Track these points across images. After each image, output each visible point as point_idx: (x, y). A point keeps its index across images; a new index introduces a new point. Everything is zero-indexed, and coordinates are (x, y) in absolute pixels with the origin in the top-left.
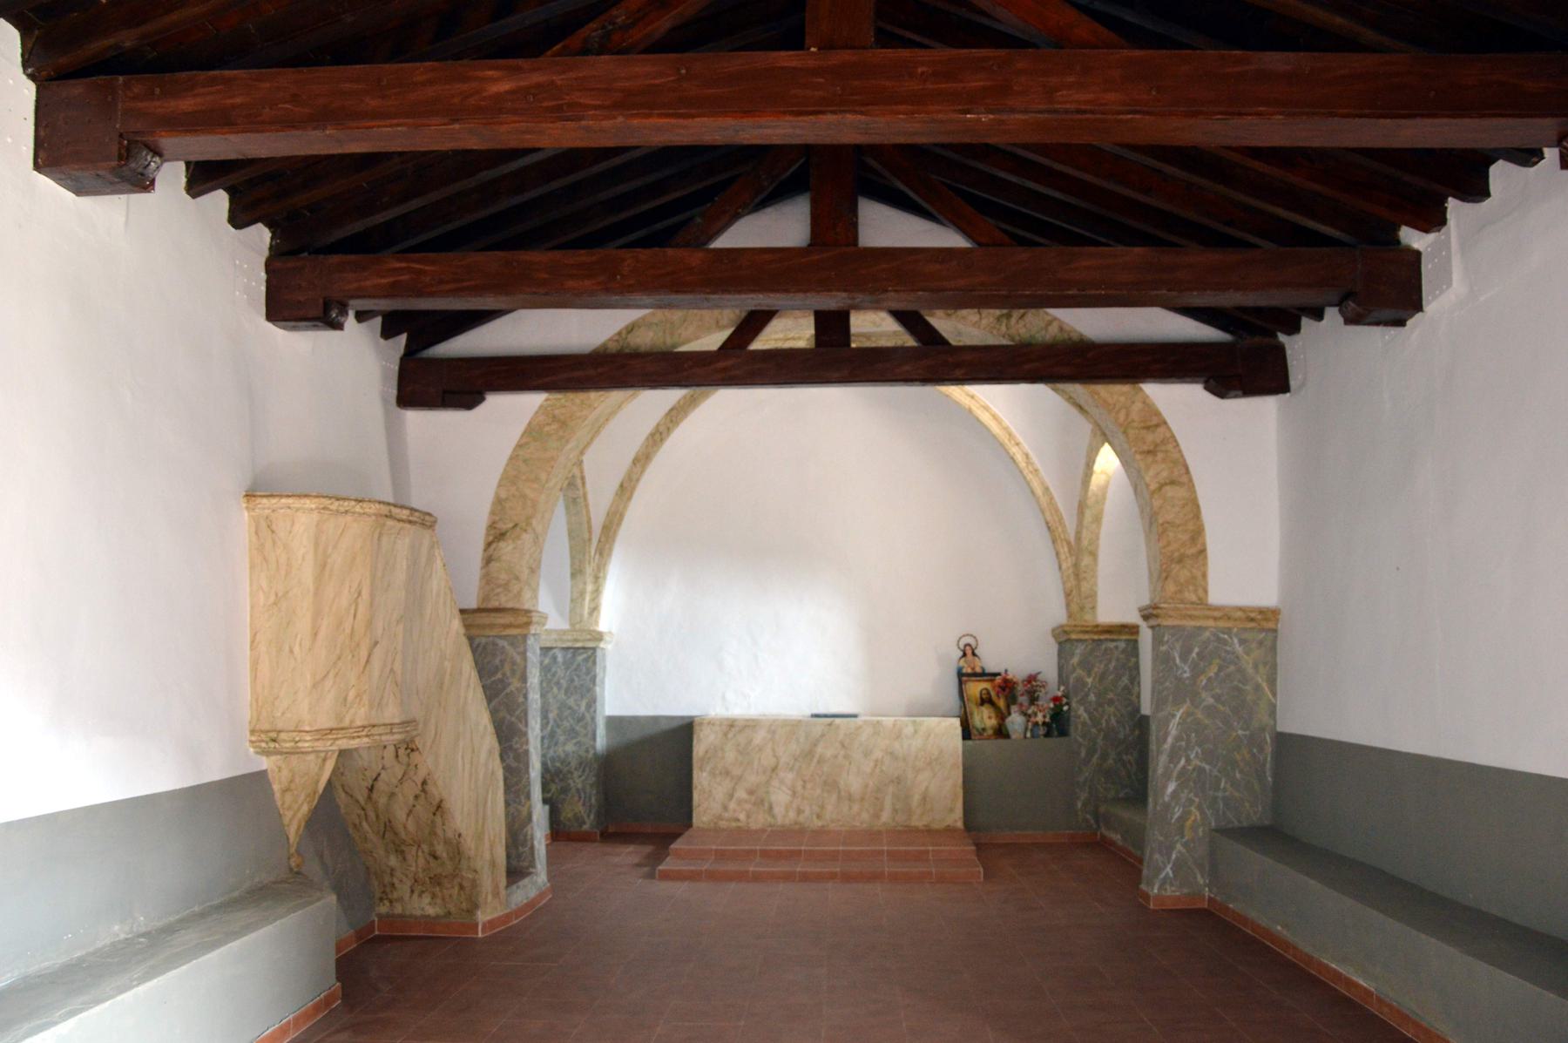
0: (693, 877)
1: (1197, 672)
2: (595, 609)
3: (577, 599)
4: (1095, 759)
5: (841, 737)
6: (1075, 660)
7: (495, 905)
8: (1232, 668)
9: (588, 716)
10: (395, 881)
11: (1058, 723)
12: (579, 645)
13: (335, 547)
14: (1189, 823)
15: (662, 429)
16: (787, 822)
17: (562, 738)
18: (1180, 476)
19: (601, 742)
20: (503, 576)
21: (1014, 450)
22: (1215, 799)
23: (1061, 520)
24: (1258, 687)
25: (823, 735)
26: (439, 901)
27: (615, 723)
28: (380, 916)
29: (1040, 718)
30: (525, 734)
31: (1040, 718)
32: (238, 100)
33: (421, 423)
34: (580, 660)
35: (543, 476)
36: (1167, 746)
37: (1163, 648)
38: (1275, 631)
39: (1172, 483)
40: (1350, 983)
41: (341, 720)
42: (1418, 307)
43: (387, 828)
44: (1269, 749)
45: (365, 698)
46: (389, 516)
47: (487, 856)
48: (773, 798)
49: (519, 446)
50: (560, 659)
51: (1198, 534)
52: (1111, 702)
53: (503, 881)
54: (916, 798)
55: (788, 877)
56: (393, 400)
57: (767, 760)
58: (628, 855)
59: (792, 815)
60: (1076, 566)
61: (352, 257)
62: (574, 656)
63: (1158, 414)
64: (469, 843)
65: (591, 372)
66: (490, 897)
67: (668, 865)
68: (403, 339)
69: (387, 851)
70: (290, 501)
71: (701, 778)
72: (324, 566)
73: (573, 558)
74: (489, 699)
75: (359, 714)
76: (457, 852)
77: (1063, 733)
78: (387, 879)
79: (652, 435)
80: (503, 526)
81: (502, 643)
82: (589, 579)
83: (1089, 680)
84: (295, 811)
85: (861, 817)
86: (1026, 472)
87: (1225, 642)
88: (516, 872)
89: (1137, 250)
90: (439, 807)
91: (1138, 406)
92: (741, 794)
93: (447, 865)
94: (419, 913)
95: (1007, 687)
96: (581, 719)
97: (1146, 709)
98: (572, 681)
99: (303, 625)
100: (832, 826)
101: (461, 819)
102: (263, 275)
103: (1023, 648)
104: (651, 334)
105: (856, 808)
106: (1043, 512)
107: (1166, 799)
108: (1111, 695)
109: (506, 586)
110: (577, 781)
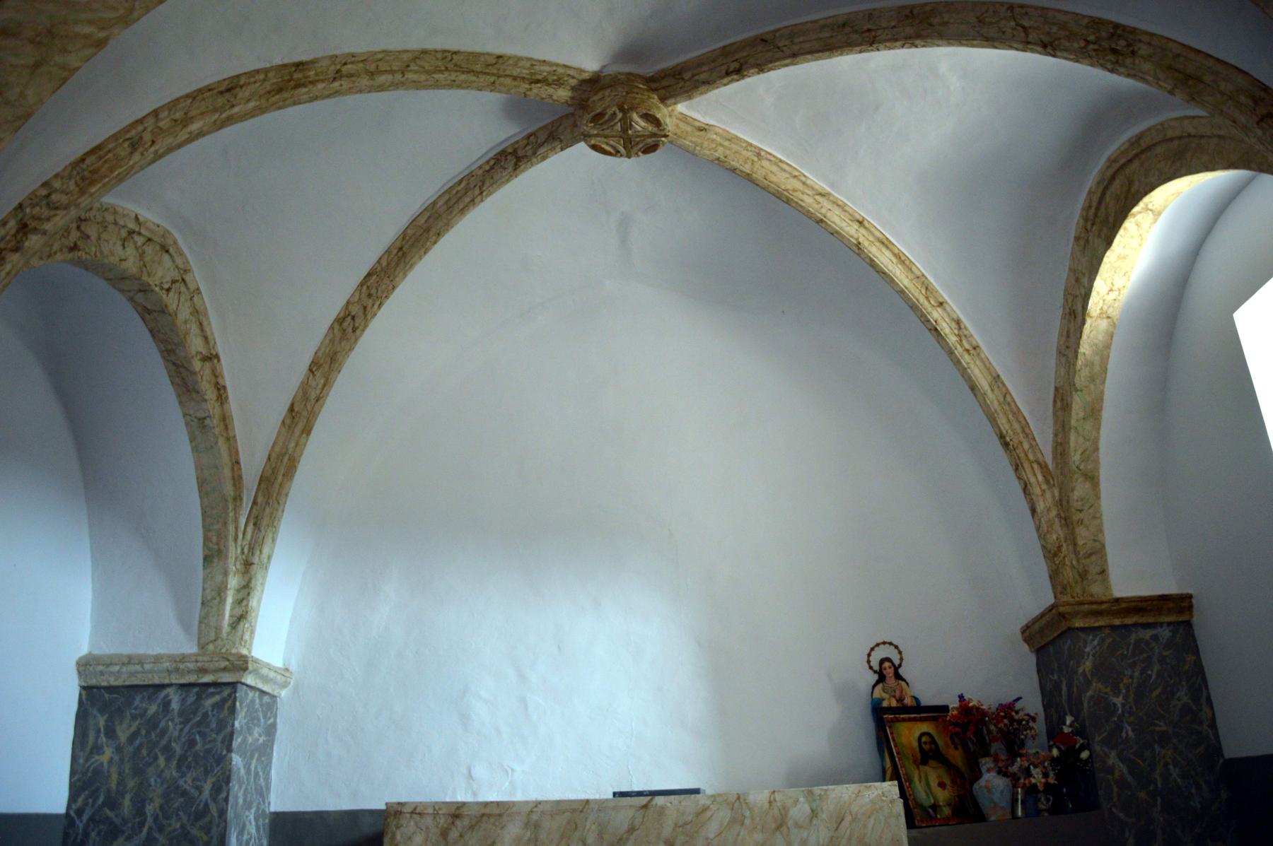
2: (241, 618)
5: (667, 831)
6: (1087, 665)
9: (214, 810)
11: (1073, 784)
12: (207, 679)
15: (355, 310)
21: (936, 315)
23: (1025, 427)
25: (632, 830)
31: (1037, 777)
50: (175, 705)
60: (1063, 504)
62: (199, 697)
73: (206, 529)
79: (340, 321)
82: (233, 565)
83: (1118, 701)
86: (959, 351)
98: (192, 743)
103: (971, 656)
106: (992, 419)
108: (1162, 727)
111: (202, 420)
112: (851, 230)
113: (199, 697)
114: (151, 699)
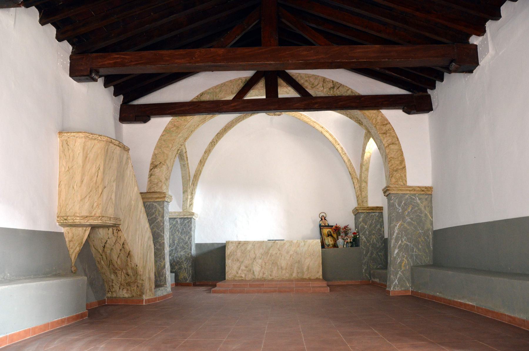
0: (224, 292)
1: (404, 210)
2: (191, 205)
3: (185, 201)
4: (369, 255)
6: (361, 220)
8: (417, 208)
9: (189, 242)
10: (114, 284)
11: (355, 242)
13: (91, 151)
14: (403, 264)
15: (214, 141)
16: (259, 277)
17: (179, 250)
18: (395, 141)
19: (194, 252)
20: (156, 181)
21: (337, 146)
22: (412, 256)
23: (354, 170)
24: (426, 215)
25: (272, 246)
26: (129, 292)
27: (199, 246)
28: (108, 298)
29: (349, 240)
30: (163, 237)
31: (349, 240)
33: (128, 128)
34: (186, 222)
35: (171, 146)
36: (394, 236)
37: (392, 202)
38: (431, 195)
39: (393, 144)
40: (465, 305)
41: (91, 213)
42: (477, 64)
43: (110, 263)
44: (431, 237)
45: (101, 207)
46: (111, 142)
47: (147, 276)
48: (254, 269)
49: (162, 135)
50: (179, 222)
51: (402, 161)
53: (153, 286)
54: (306, 268)
55: (259, 292)
57: (253, 256)
59: (261, 275)
60: (360, 187)
61: (101, 54)
62: (184, 220)
63: (387, 120)
64: (140, 269)
65: (187, 108)
66: (148, 291)
68: (121, 97)
69: (111, 273)
70: (75, 134)
71: (228, 262)
72: (86, 157)
74: (150, 225)
75: (98, 212)
77: (357, 246)
78: (111, 284)
79: (211, 143)
80: (156, 163)
81: (155, 204)
83: (366, 227)
85: (286, 275)
87: (414, 199)
89: (378, 46)
90: (129, 254)
91: (380, 117)
92: (243, 267)
93: (132, 278)
94: (122, 296)
95: (337, 229)
96: (187, 242)
97: (386, 236)
98: (183, 229)
99: (78, 178)
101: (137, 259)
102: (69, 61)
103: (342, 216)
104: (209, 96)
105: (284, 272)
106: (348, 168)
107: (395, 256)
108: (374, 232)
110: (185, 265)
111: (184, 165)
112: (320, 129)
113: (184, 220)
114: (174, 221)
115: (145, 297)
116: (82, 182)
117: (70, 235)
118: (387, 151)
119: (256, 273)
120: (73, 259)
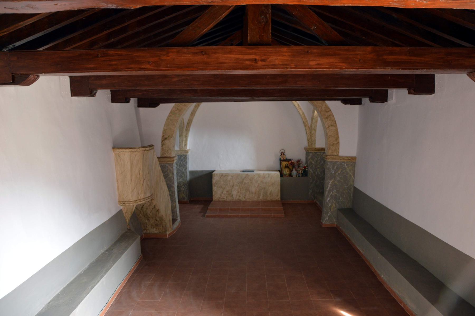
0: (214, 217)
2: (186, 145)
6: (310, 157)
7: (171, 229)
11: (305, 173)
18: (334, 124)
23: (307, 121)
24: (350, 175)
27: (192, 172)
28: (144, 233)
29: (300, 172)
32: (116, 81)
34: (183, 158)
39: (332, 126)
40: (360, 252)
44: (352, 190)
48: (233, 193)
49: (169, 116)
51: (337, 138)
52: (318, 168)
53: (172, 224)
56: (137, 106)
58: (197, 208)
59: (238, 197)
60: (310, 133)
63: (329, 108)
67: (208, 213)
71: (214, 188)
72: (132, 164)
75: (142, 196)
76: (162, 219)
77: (306, 175)
82: (184, 137)
84: (128, 216)
88: (174, 220)
92: (225, 192)
93: (159, 222)
96: (183, 173)
100: (248, 200)
101: (162, 213)
103: (296, 153)
108: (319, 166)
109: (167, 151)
115: (168, 233)
116: (131, 180)
117: (126, 209)
118: (327, 131)
119: (234, 196)
120: (127, 221)
